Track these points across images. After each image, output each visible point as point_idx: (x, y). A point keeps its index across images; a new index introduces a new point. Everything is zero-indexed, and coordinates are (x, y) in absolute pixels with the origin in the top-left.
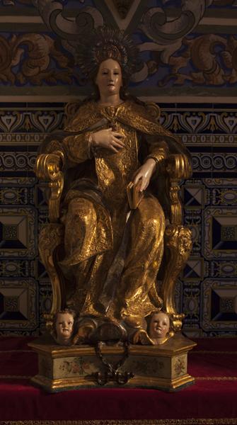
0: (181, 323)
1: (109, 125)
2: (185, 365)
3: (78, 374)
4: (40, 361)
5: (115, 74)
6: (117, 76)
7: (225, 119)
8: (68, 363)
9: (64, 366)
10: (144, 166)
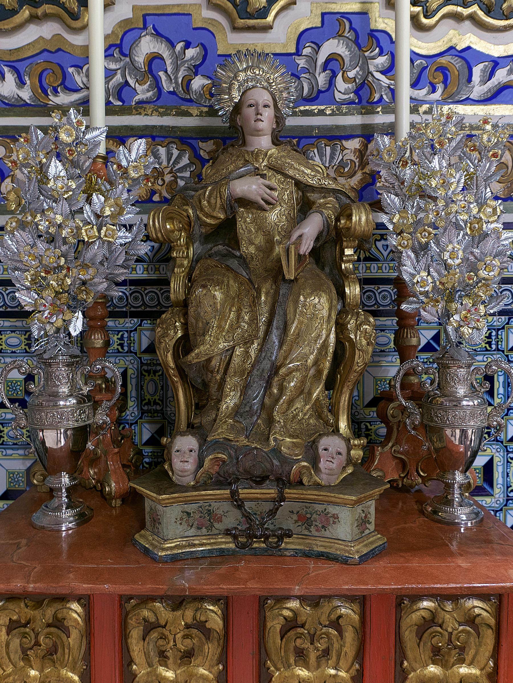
0: (361, 453)
1: (257, 172)
2: (372, 519)
3: (204, 530)
4: (147, 509)
5: (265, 106)
6: (267, 109)
7: (377, 242)
8: (189, 514)
9: (182, 519)
10: (306, 221)
